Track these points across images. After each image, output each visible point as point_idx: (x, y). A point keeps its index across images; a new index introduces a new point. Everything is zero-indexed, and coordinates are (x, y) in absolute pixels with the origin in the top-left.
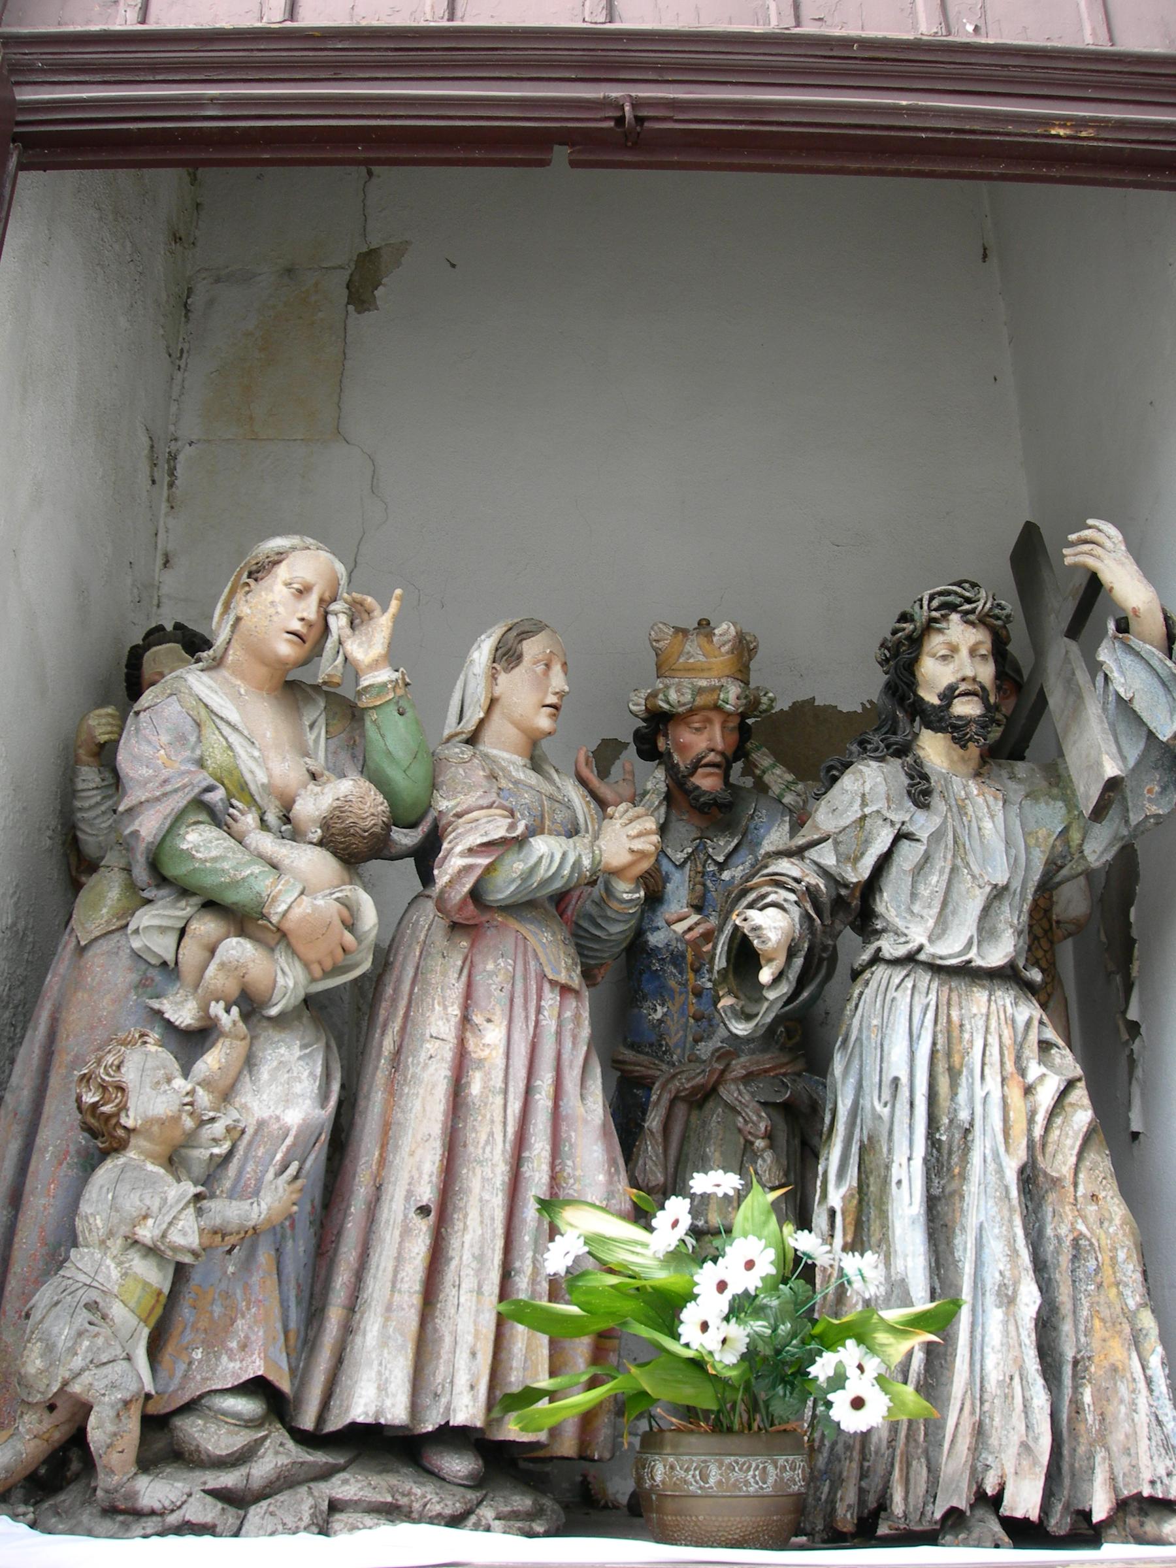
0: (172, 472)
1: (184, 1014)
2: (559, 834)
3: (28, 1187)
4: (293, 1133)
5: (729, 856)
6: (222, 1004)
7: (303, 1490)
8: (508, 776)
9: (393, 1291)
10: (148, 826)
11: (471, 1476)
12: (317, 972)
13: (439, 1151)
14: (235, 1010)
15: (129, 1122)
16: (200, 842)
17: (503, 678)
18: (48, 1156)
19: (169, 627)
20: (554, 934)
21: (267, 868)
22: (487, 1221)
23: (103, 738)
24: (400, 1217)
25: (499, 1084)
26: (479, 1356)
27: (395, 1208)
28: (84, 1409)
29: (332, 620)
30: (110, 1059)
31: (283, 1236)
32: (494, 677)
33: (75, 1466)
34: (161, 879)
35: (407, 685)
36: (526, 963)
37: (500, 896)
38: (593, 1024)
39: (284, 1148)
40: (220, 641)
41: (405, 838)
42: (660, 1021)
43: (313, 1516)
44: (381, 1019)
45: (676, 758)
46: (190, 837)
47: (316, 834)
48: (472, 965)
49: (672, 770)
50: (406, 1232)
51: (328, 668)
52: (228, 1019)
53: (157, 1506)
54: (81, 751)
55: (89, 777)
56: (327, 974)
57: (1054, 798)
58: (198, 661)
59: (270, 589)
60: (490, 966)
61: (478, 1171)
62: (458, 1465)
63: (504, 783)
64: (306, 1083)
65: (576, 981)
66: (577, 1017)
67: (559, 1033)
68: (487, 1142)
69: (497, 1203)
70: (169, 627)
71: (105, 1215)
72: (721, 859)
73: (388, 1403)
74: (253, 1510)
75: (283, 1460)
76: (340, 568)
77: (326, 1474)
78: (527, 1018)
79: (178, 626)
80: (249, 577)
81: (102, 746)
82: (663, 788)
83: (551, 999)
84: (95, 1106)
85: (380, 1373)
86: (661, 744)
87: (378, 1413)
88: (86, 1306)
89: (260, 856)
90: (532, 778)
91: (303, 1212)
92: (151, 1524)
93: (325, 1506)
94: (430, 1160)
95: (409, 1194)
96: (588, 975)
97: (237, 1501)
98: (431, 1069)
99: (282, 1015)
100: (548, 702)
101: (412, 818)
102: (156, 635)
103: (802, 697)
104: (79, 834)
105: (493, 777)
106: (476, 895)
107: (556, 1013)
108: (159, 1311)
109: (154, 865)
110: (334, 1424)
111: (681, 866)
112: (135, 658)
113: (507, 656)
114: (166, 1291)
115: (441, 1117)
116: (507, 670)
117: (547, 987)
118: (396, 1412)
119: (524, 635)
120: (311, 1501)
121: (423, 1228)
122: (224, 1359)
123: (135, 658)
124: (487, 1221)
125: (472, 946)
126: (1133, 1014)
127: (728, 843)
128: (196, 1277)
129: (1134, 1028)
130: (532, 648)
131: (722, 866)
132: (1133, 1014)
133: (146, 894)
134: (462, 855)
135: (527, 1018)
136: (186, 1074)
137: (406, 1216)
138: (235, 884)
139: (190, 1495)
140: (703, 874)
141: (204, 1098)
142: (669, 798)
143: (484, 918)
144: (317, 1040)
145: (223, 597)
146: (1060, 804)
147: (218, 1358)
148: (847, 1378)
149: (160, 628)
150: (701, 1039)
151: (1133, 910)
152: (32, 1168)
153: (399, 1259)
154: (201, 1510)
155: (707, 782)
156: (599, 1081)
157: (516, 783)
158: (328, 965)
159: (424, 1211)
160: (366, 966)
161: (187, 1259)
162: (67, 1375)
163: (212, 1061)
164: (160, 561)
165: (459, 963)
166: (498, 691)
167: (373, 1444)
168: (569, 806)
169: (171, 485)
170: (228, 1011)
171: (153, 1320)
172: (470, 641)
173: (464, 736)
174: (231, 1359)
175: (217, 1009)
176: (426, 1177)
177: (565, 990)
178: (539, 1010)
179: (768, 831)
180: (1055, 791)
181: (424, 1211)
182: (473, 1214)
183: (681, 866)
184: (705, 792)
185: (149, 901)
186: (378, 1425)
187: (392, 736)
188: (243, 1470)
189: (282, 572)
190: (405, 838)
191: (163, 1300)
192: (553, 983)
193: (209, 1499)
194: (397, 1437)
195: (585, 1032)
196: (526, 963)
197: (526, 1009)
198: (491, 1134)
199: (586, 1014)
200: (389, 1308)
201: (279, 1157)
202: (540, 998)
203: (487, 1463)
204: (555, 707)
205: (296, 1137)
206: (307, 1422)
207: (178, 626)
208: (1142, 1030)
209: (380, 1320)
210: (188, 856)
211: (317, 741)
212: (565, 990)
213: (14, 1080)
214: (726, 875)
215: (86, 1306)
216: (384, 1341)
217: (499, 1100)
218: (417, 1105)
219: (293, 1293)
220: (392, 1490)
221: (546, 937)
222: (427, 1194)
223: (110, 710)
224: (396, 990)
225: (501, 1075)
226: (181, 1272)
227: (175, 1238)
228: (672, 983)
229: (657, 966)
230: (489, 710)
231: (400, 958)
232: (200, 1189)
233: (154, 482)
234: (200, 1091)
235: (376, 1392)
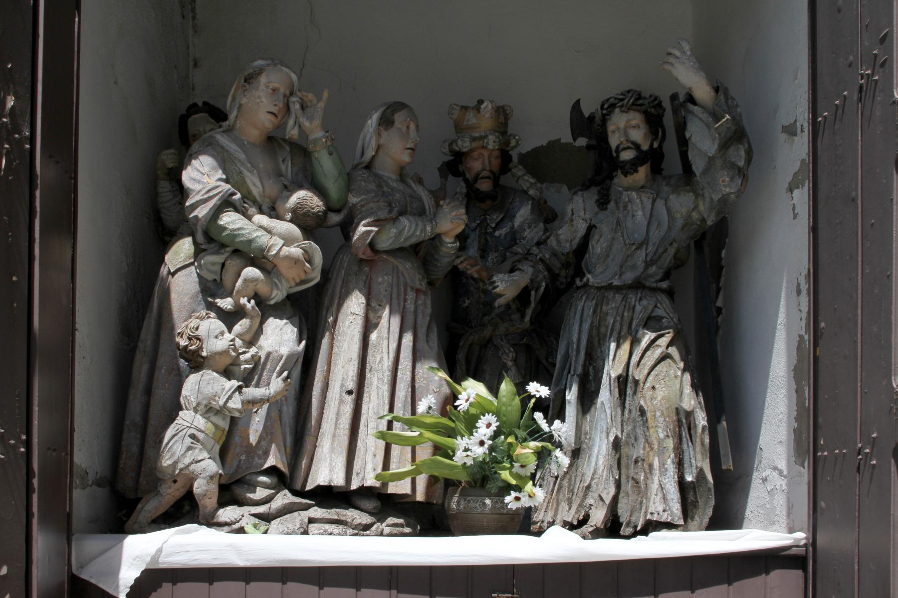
0: (193, 10)
1: (226, 303)
2: (415, 215)
3: (154, 386)
4: (284, 358)
5: (497, 224)
6: (246, 298)
7: (296, 514)
8: (388, 186)
9: (335, 429)
10: (202, 212)
11: (375, 508)
12: (293, 284)
13: (357, 366)
14: (253, 301)
15: (204, 354)
16: (230, 220)
17: (385, 134)
18: (163, 371)
19: (200, 104)
20: (412, 264)
21: (265, 233)
22: (381, 397)
23: (171, 165)
24: (338, 396)
25: (386, 335)
26: (377, 456)
27: (335, 392)
28: (192, 479)
29: (291, 105)
30: (192, 325)
31: (282, 404)
32: (379, 135)
33: (187, 508)
34: (210, 239)
35: (333, 139)
36: (398, 278)
37: (384, 245)
38: (432, 307)
39: (280, 364)
40: (232, 117)
41: (335, 218)
42: (467, 307)
43: (301, 524)
44: (326, 305)
45: (467, 176)
46: (224, 219)
47: (289, 216)
48: (371, 279)
49: (466, 181)
50: (341, 402)
51: (293, 132)
52: (250, 305)
53: (228, 520)
54: (159, 172)
55: (165, 186)
56: (298, 285)
57: (688, 192)
58: (220, 127)
59: (257, 89)
60: (380, 280)
61: (376, 375)
62: (370, 504)
63: (385, 189)
64: (290, 335)
65: (423, 286)
66: (424, 304)
67: (415, 312)
68: (380, 362)
69: (385, 389)
70: (200, 104)
71: (195, 396)
72: (493, 225)
73: (335, 476)
74: (273, 522)
75: (286, 501)
76: (294, 77)
77: (307, 508)
78: (399, 304)
79: (205, 103)
80: (245, 81)
81: (170, 169)
82: (465, 190)
83: (411, 296)
84: (186, 347)
85: (330, 464)
86: (461, 168)
87: (330, 481)
88: (189, 436)
89: (260, 227)
90: (401, 187)
91: (292, 393)
92: (226, 528)
93: (306, 520)
94: (352, 370)
95: (342, 386)
96: (430, 283)
97: (266, 518)
98: (352, 328)
99: (276, 304)
100: (409, 146)
101: (338, 207)
102: (193, 109)
103: (553, 138)
104: (162, 215)
105: (379, 186)
106: (372, 245)
107: (414, 301)
108: (224, 438)
109: (206, 234)
110: (309, 487)
111: (475, 229)
112: (183, 121)
113: (386, 122)
114: (227, 429)
115: (357, 350)
116: (386, 129)
117: (409, 289)
118: (339, 480)
119: (394, 112)
120: (300, 518)
121: (350, 400)
122: (256, 459)
123: (183, 121)
124: (381, 397)
125: (371, 270)
126: (719, 303)
127: (498, 217)
128: (241, 424)
129: (719, 310)
130: (400, 118)
131: (495, 229)
132: (719, 303)
133: (203, 247)
134: (364, 226)
135: (399, 304)
136: (230, 332)
137: (341, 395)
138: (250, 242)
139: (243, 516)
140: (486, 233)
141: (238, 342)
142: (467, 195)
143: (376, 257)
144: (294, 316)
145: (232, 93)
146: (691, 194)
147: (253, 459)
148: (693, 592)
149: (195, 105)
150: (486, 315)
151: (724, 252)
152: (155, 377)
153: (338, 414)
154: (248, 522)
155: (485, 186)
156: (436, 334)
157: (392, 189)
158: (298, 281)
159: (350, 392)
160: (318, 280)
161: (237, 414)
162: (182, 466)
163: (241, 326)
164: (191, 64)
165: (364, 278)
166: (382, 141)
167: (327, 496)
168: (421, 200)
169: (194, 18)
170: (249, 301)
171: (221, 442)
172: (368, 116)
173: (364, 165)
174: (259, 459)
175: (243, 301)
176: (350, 377)
177: (418, 291)
178: (405, 300)
179: (519, 210)
180: (688, 188)
181: (350, 392)
182: (374, 394)
183: (475, 229)
184: (482, 192)
185: (205, 250)
186: (330, 486)
187: (327, 166)
188: (268, 506)
189: (263, 79)
190: (335, 218)
191: (226, 433)
192: (412, 288)
193: (252, 518)
194: (339, 493)
195: (429, 310)
196: (398, 278)
197: (398, 299)
198: (382, 358)
199: (429, 302)
200: (334, 436)
201: (278, 368)
202: (405, 295)
203: (382, 504)
204: (412, 149)
205: (286, 359)
206: (298, 487)
207: (205, 103)
208: (723, 311)
209: (330, 441)
210: (224, 229)
211: (287, 167)
212: (418, 291)
213: (142, 336)
214: (497, 233)
215: (189, 436)
216: (332, 450)
217: (386, 342)
218: (346, 345)
219: (288, 430)
220: (337, 514)
221: (408, 265)
222: (351, 385)
223: (172, 151)
224: (333, 291)
225: (386, 331)
226: (233, 420)
227: (231, 404)
228: (472, 288)
229: (464, 281)
230: (377, 151)
231: (335, 276)
232: (241, 383)
233: (183, 17)
234: (237, 339)
235: (327, 470)
